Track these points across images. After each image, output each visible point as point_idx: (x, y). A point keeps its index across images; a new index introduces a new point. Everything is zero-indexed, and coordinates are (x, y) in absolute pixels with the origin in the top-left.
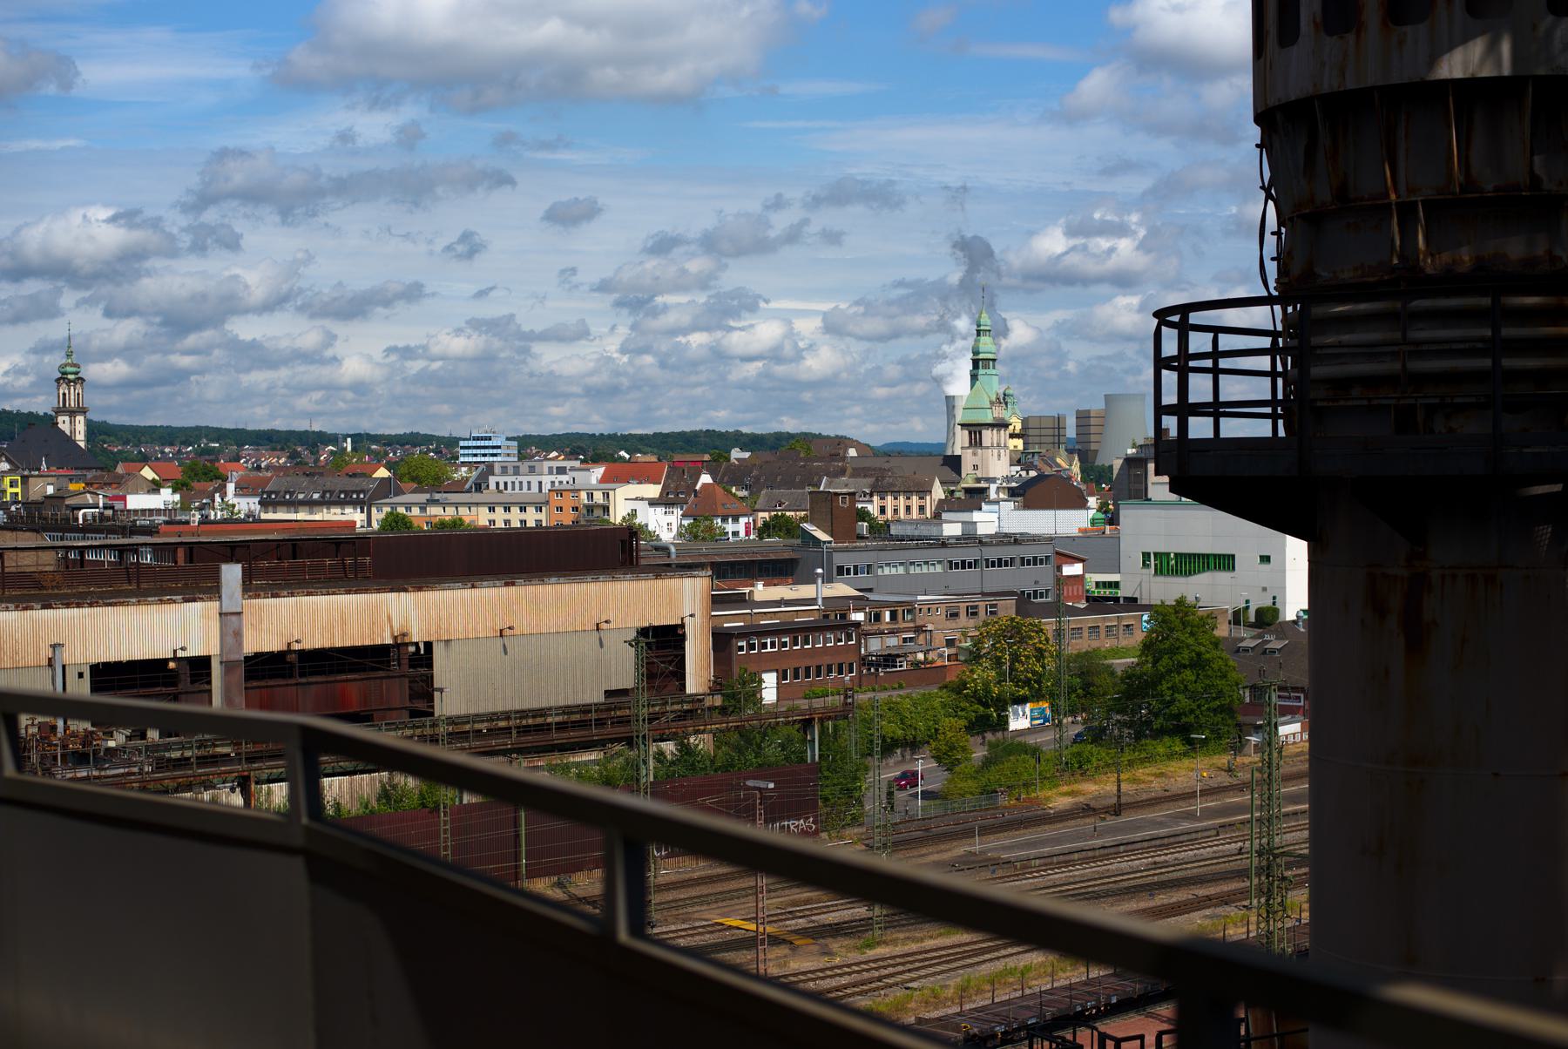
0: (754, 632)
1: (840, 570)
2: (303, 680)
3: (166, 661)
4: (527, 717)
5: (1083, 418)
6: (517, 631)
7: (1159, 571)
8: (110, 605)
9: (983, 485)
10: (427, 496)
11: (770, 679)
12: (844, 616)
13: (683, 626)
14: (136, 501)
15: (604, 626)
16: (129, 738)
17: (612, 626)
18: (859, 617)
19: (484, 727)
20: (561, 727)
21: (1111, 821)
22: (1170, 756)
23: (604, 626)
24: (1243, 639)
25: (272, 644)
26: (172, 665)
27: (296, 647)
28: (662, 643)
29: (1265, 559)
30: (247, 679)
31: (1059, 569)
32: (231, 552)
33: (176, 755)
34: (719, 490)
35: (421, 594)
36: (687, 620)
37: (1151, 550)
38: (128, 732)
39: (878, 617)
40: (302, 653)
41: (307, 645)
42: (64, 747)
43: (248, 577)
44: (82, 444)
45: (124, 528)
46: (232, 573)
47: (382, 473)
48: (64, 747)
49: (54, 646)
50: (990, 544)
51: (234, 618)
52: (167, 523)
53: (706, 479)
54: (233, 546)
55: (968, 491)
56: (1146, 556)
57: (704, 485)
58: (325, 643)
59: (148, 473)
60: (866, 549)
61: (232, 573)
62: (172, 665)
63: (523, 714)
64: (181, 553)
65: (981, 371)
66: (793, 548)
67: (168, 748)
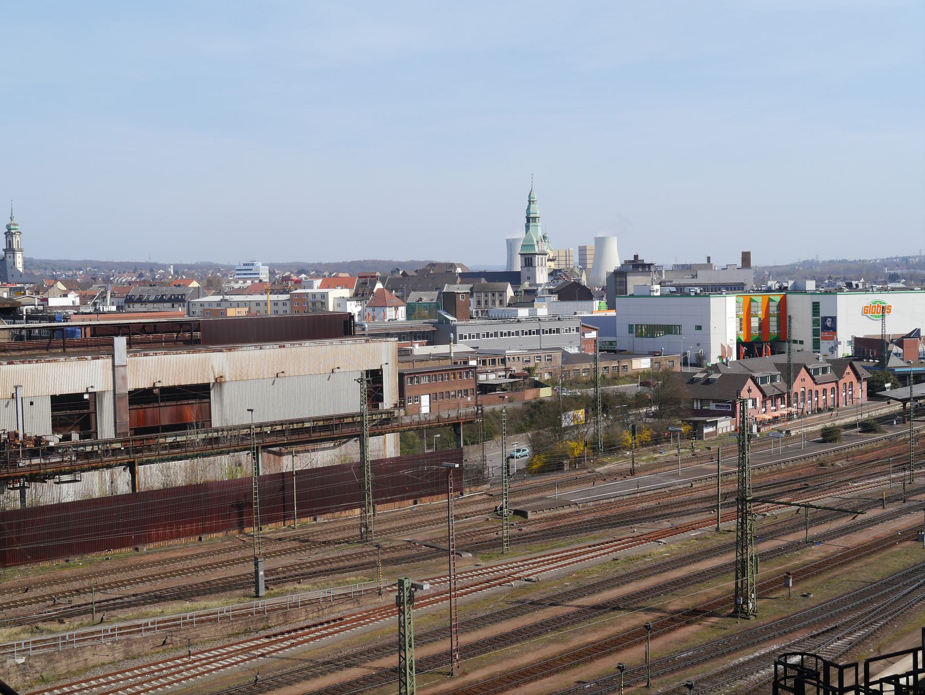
0: (414, 375)
1: (461, 337)
2: (162, 404)
3: (82, 394)
4: (293, 423)
5: (582, 251)
6: (286, 374)
7: (640, 335)
8: (49, 361)
9: (533, 288)
10: (221, 297)
11: (425, 400)
12: (466, 363)
13: (381, 370)
14: (53, 302)
15: (336, 370)
16: (60, 440)
17: (341, 370)
18: (473, 363)
19: (268, 430)
20: (314, 429)
21: (631, 479)
22: (913, 257)
23: (336, 370)
24: (695, 374)
25: (144, 384)
26: (86, 397)
27: (158, 385)
28: (374, 378)
29: (699, 328)
30: (130, 404)
31: (583, 335)
32: (119, 330)
33: (89, 449)
34: (386, 292)
35: (231, 353)
36: (384, 367)
37: (634, 323)
38: (60, 436)
39: (484, 362)
40: (163, 389)
41: (165, 384)
42: (24, 446)
43: (130, 344)
44: (21, 270)
45: (50, 317)
46: (120, 342)
47: (195, 284)
48: (24, 446)
49: (631, 331)
50: (545, 321)
51: (122, 369)
52: (75, 314)
53: (379, 286)
54: (120, 326)
55: (526, 291)
56: (631, 326)
57: (378, 289)
58: (176, 383)
59: (60, 286)
60: (475, 325)
61: (120, 342)
62: (86, 397)
63: (291, 422)
64: (88, 329)
65: (531, 224)
66: (434, 324)
67: (85, 445)
